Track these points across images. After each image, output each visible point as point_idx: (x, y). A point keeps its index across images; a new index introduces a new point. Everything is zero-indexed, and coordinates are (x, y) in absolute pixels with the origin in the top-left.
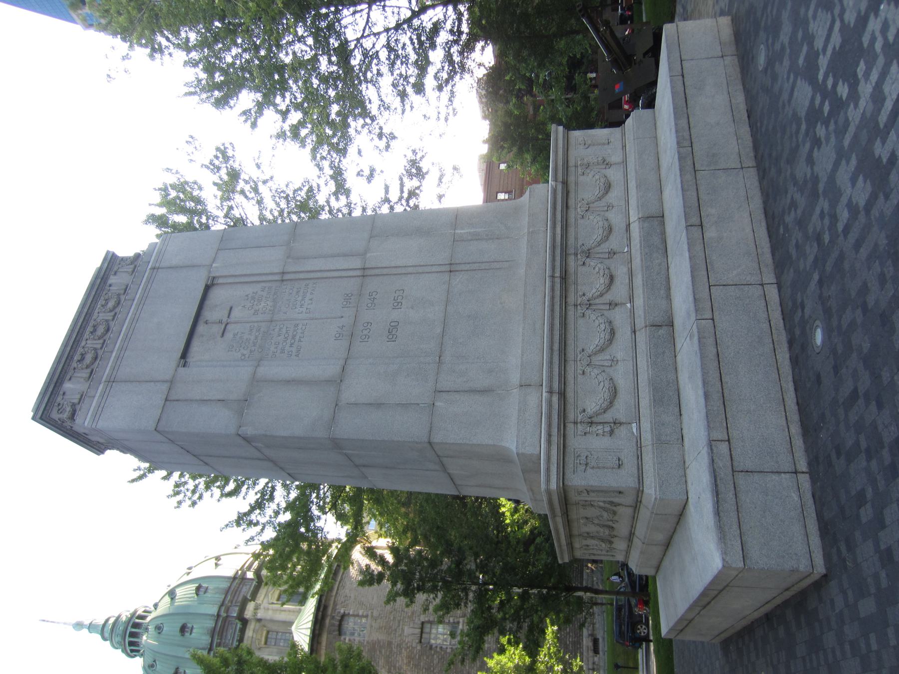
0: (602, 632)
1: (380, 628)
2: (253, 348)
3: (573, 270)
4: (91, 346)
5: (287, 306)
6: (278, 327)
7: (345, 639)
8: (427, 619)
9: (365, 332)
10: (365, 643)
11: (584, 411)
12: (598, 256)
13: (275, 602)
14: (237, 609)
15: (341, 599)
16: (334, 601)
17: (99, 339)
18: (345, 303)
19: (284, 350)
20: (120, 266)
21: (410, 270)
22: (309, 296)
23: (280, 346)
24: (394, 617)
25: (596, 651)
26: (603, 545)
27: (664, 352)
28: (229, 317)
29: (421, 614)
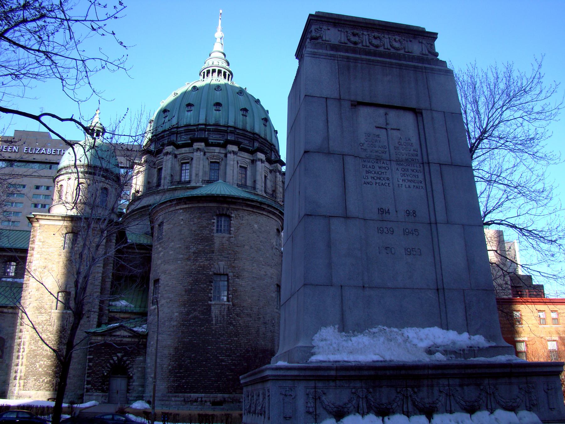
1: (223, 244)
7: (214, 219)
8: (230, 278)
9: (385, 230)
10: (212, 234)
12: (448, 402)
14: (233, 139)
15: (241, 213)
16: (239, 209)
17: (370, 43)
19: (369, 173)
20: (427, 45)
21: (437, 258)
22: (412, 184)
23: (371, 170)
26: (248, 407)
28: (391, 129)
29: (233, 273)
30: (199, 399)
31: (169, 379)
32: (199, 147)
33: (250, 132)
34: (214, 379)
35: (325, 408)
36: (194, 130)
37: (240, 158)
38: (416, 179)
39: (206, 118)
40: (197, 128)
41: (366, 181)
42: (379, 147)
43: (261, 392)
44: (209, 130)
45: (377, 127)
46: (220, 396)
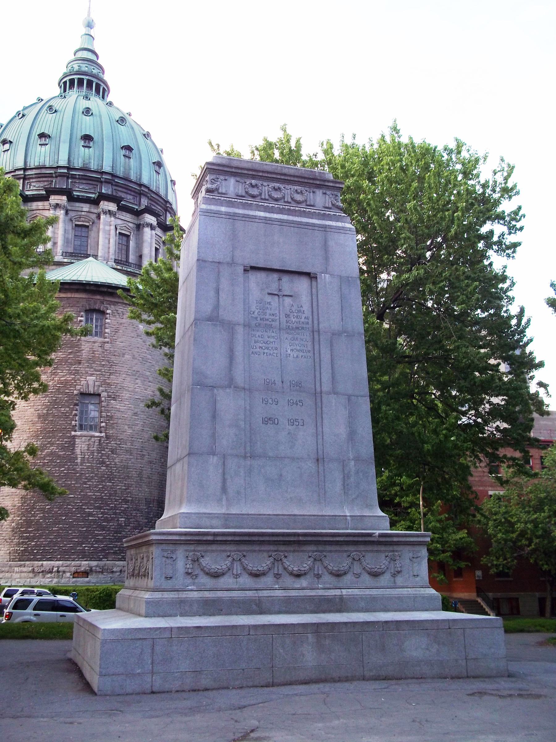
0: (94, 581)
2: (259, 319)
4: (263, 191)
6: (275, 335)
9: (270, 401)
11: (202, 557)
13: (118, 232)
21: (320, 429)
24: (104, 365)
25: (76, 574)
27: (240, 608)
29: (108, 392)
30: (55, 569)
31: (12, 542)
32: (59, 202)
33: (135, 183)
34: (76, 540)
35: (202, 570)
36: (50, 176)
37: (119, 222)
38: (305, 348)
39: (69, 158)
40: (55, 173)
41: (254, 350)
42: (270, 315)
43: (145, 555)
44: (73, 177)
45: (269, 294)
46: (85, 564)
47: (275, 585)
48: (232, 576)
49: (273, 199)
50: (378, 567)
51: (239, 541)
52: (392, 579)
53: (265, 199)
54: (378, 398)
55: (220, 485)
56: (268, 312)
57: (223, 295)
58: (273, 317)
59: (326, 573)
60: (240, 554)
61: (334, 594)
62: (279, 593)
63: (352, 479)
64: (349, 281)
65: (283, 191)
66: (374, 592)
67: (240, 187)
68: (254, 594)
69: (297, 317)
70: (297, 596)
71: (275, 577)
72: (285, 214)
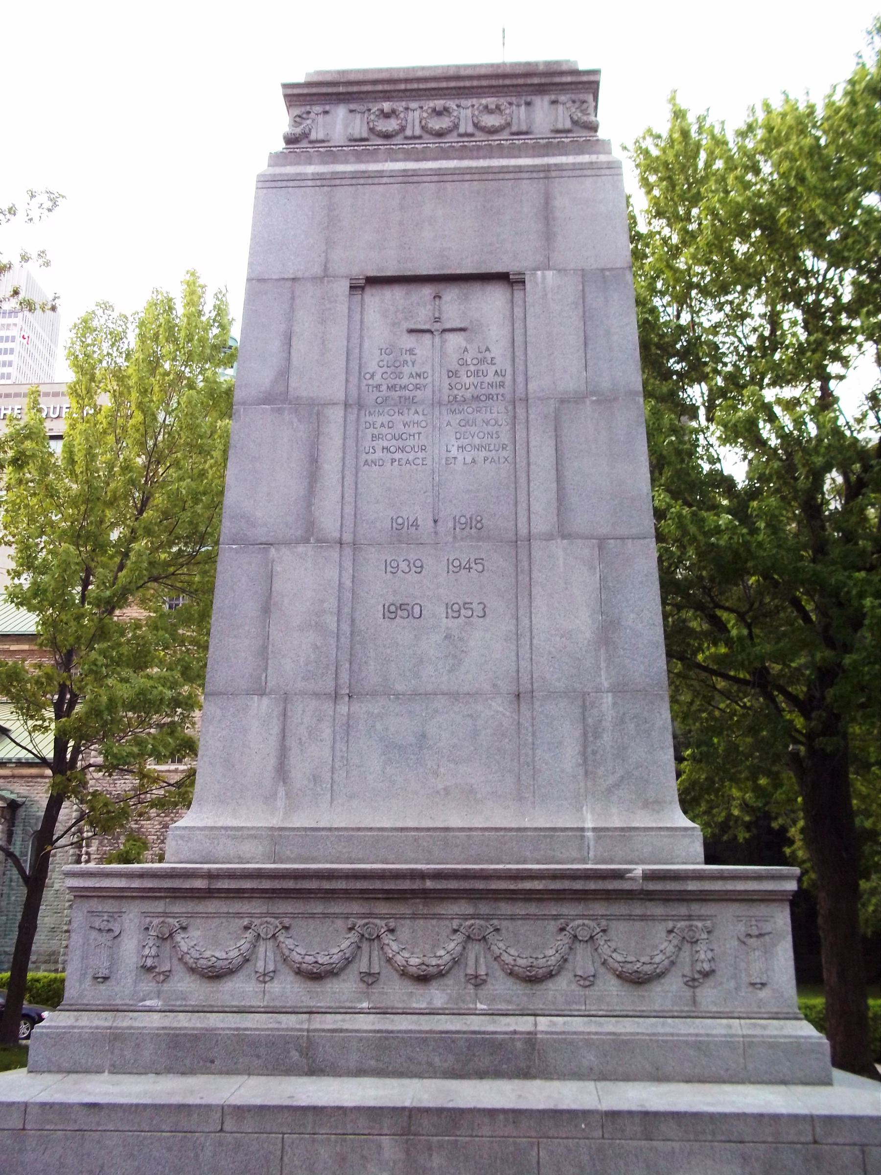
3: (442, 912)
5: (463, 423)
6: (421, 418)
9: (403, 566)
11: (184, 929)
17: (423, 128)
18: (463, 520)
20: (569, 104)
27: (258, 1057)
38: (494, 441)
41: (370, 457)
42: (411, 376)
45: (411, 331)
47: (360, 1001)
48: (254, 977)
49: (431, 134)
50: (643, 960)
51: (274, 891)
52: (688, 993)
53: (414, 137)
54: (855, 585)
55: (272, 761)
56: (406, 370)
57: (299, 347)
58: (418, 381)
59: (499, 973)
60: (277, 922)
61: (511, 1029)
62: (366, 1023)
63: (607, 738)
64: (604, 277)
65: (455, 114)
66: (627, 1027)
67: (358, 121)
68: (302, 1023)
69: (476, 374)
70: (410, 1031)
71: (362, 980)
72: (454, 159)
